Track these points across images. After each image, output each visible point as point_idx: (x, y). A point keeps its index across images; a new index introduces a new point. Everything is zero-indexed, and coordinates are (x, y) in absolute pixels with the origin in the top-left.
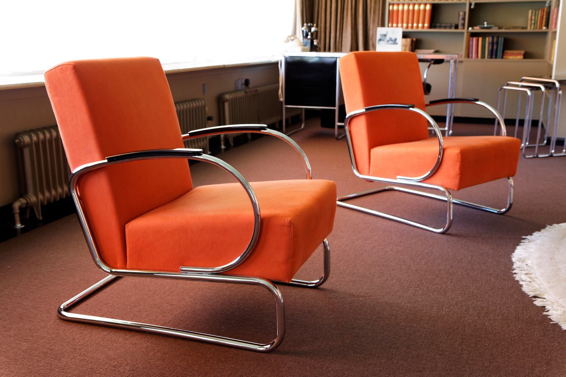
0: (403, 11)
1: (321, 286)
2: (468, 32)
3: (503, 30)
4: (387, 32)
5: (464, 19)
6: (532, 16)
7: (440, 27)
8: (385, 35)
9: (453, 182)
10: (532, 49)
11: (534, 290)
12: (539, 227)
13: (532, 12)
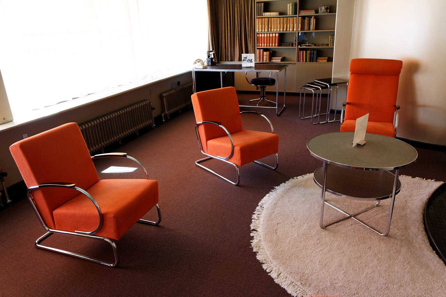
1: (159, 224)
5: (296, 41)
6: (331, 39)
7: (284, 45)
8: (246, 58)
12: (285, 179)
13: (331, 37)
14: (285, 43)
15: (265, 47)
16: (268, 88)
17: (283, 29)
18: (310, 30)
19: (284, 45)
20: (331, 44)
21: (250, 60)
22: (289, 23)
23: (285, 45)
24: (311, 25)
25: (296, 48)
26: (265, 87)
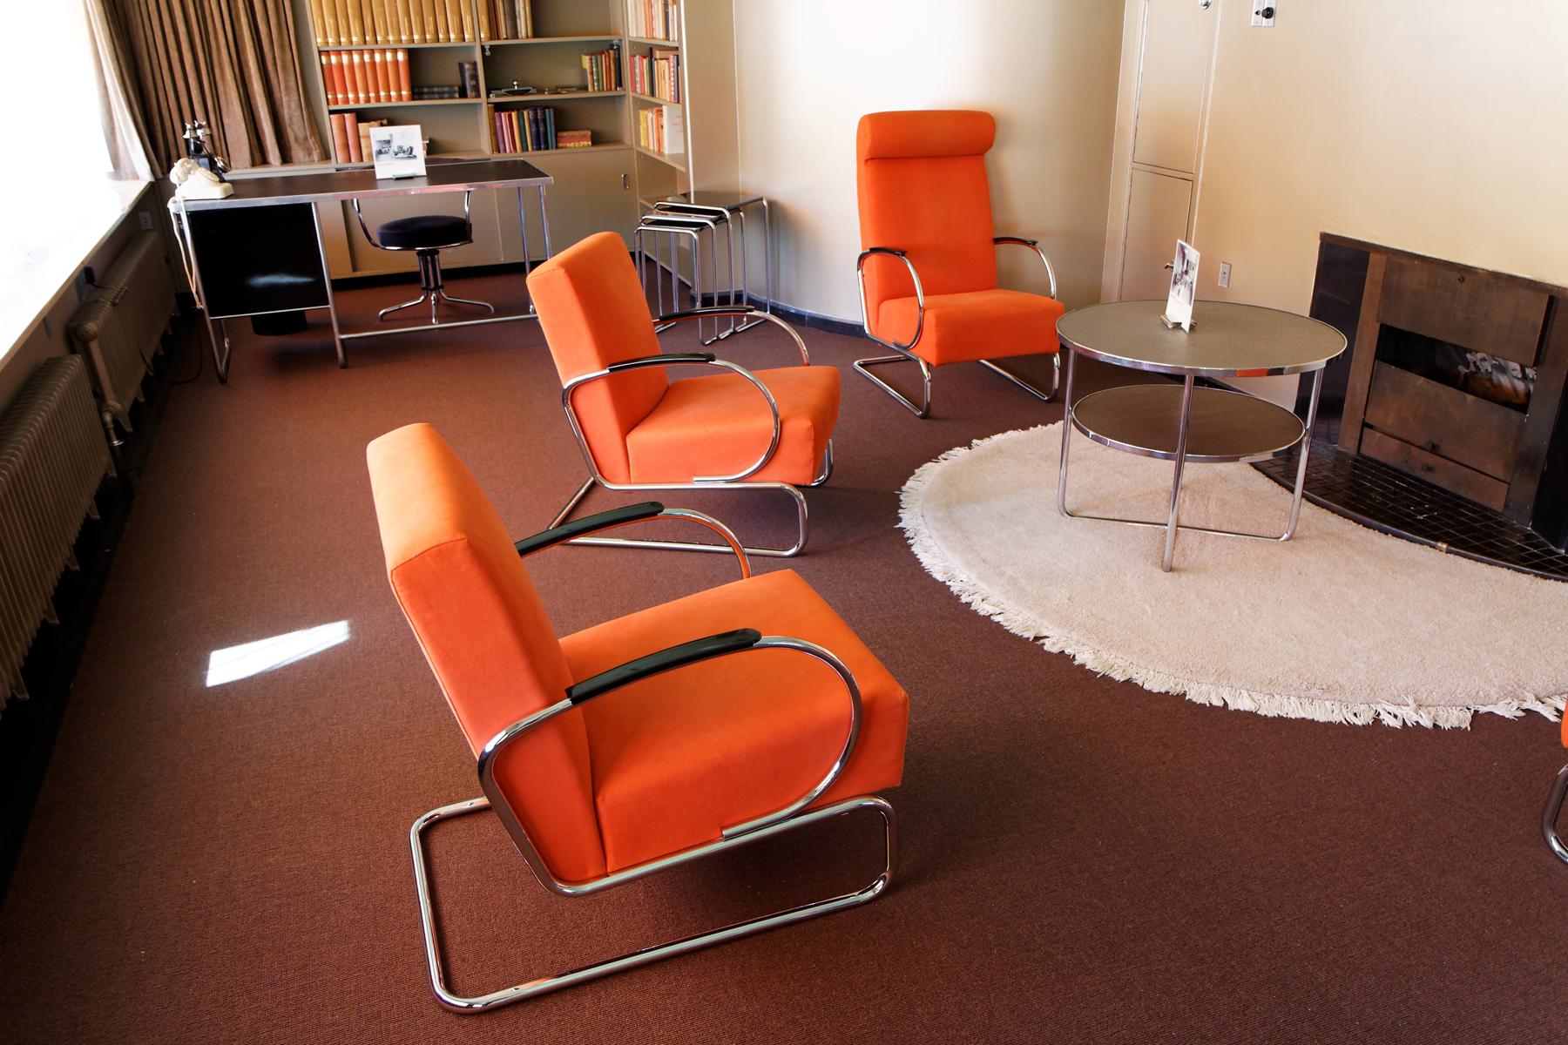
3: (546, 97)
4: (391, 135)
5: (475, 77)
7: (431, 96)
8: (388, 142)
10: (601, 125)
13: (591, 59)
14: (432, 87)
15: (362, 105)
16: (451, 256)
17: (424, 32)
18: (517, 37)
19: (428, 93)
20: (595, 84)
21: (404, 152)
22: (431, 11)
23: (433, 93)
24: (518, 20)
25: (481, 104)
26: (438, 253)
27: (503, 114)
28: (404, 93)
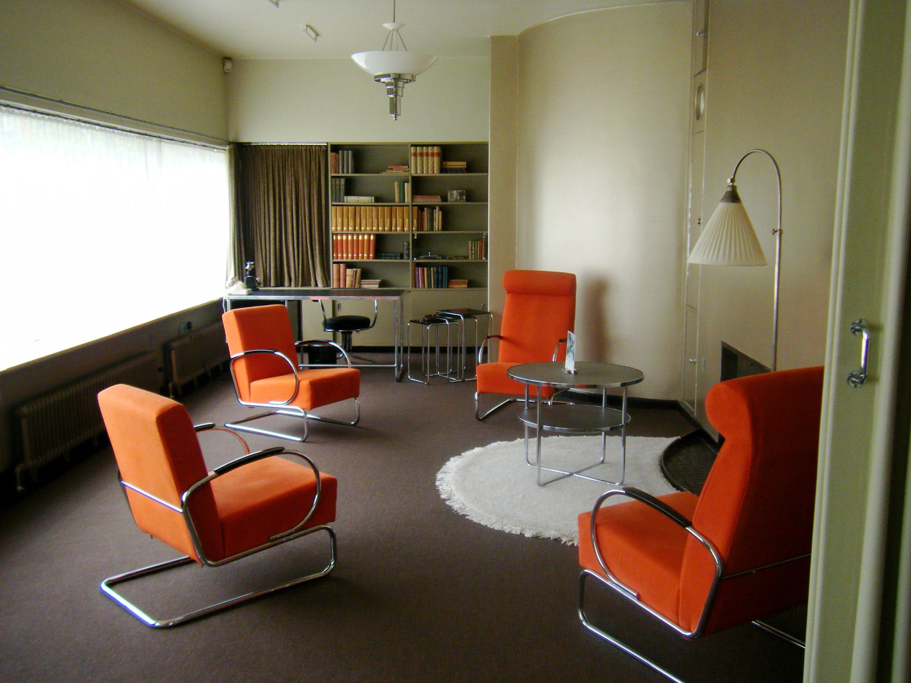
0: (342, 240)
2: (412, 263)
5: (408, 249)
6: (472, 247)
9: (308, 404)
11: (593, 526)
13: (472, 243)
15: (349, 260)
17: (384, 227)
27: (420, 268)
28: (371, 255)
